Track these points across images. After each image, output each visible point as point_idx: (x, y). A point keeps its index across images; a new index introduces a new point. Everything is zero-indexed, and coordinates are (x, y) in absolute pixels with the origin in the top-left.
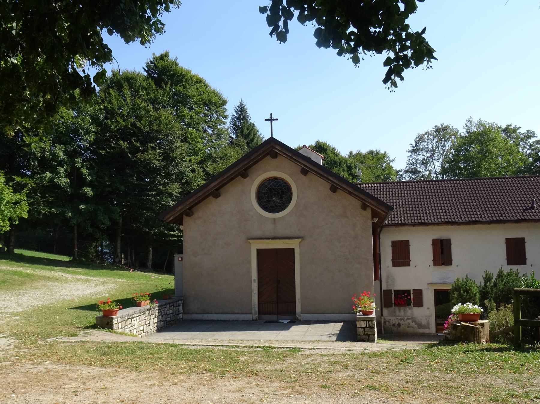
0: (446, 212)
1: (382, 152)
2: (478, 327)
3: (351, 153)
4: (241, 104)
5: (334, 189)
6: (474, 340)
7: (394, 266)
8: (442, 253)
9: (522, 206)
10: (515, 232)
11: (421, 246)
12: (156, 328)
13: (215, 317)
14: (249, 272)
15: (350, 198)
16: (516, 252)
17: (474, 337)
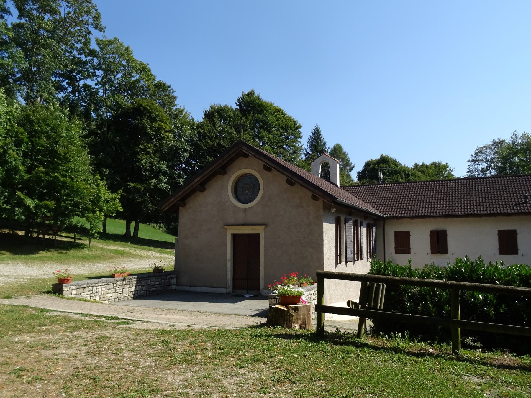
0: (443, 207)
1: (444, 163)
2: (290, 310)
3: (416, 165)
4: (316, 128)
5: (290, 183)
6: (284, 324)
7: (396, 253)
8: (439, 242)
9: (515, 201)
10: (507, 225)
11: (420, 237)
12: (132, 296)
13: (198, 289)
14: (225, 253)
15: (305, 190)
16: (508, 243)
17: (284, 321)
